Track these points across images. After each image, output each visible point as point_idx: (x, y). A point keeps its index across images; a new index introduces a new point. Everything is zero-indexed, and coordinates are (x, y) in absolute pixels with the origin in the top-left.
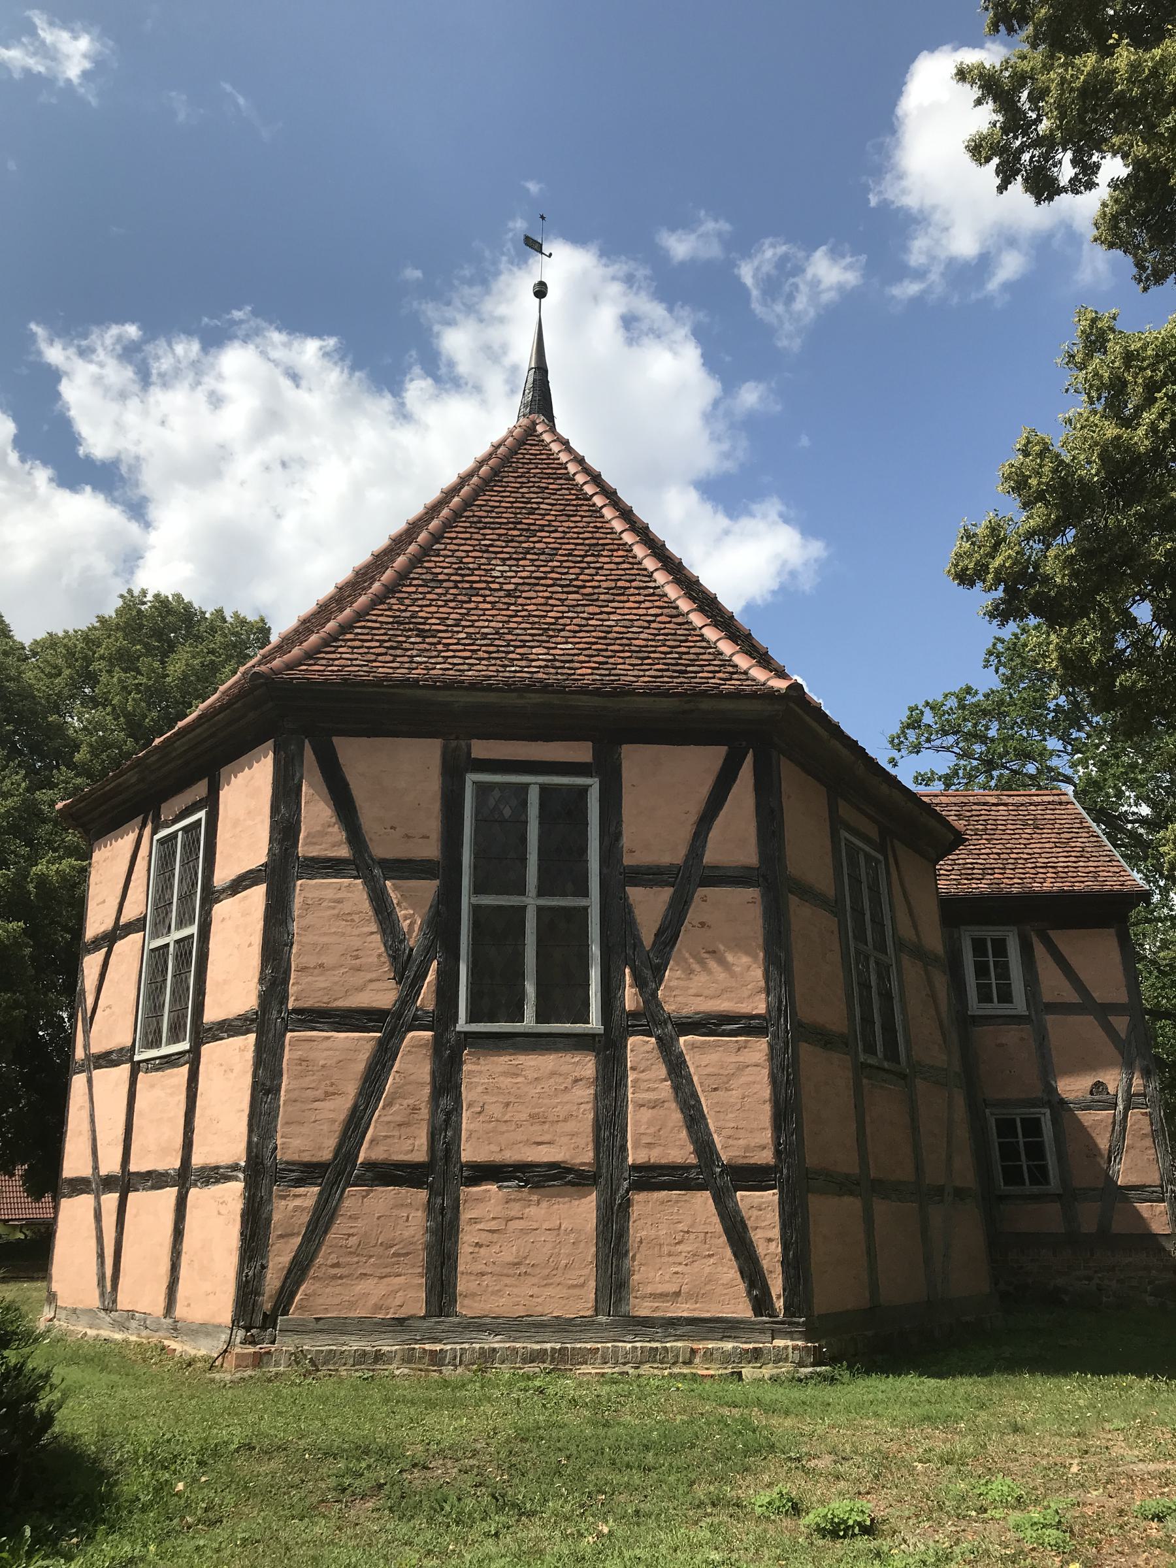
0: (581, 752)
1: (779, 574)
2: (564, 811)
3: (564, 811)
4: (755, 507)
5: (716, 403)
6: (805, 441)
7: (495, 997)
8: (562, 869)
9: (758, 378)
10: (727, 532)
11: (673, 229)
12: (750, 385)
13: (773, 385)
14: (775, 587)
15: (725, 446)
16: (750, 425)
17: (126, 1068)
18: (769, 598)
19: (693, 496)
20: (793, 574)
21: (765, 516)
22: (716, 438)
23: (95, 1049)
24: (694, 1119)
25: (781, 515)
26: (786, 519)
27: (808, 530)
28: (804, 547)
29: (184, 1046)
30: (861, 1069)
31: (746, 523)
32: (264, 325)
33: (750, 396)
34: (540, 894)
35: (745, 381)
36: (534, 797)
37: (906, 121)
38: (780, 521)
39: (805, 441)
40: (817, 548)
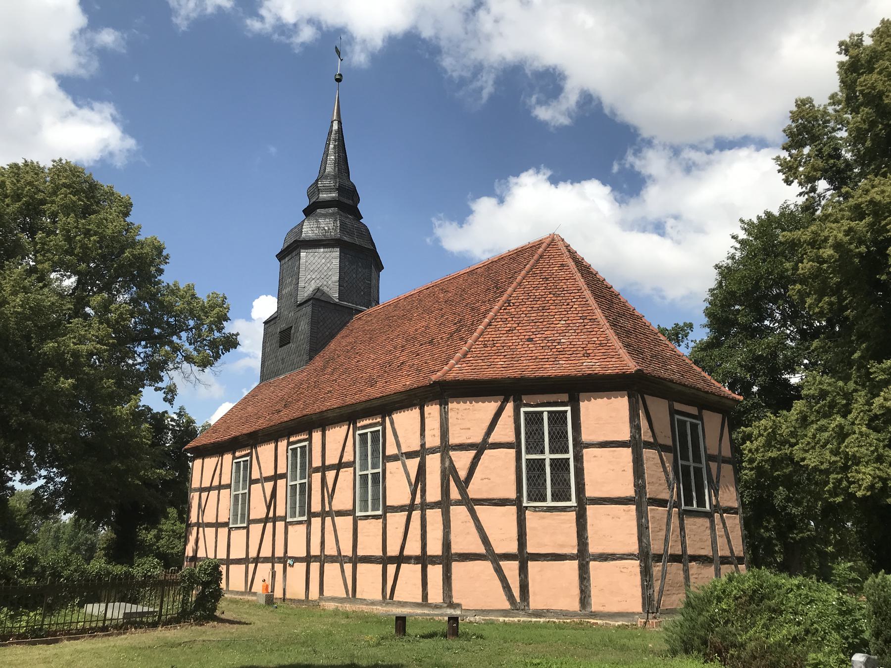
0: (565, 397)
1: (102, 151)
2: (557, 419)
3: (557, 419)
4: (97, 105)
5: (82, 31)
6: (137, 78)
7: (537, 495)
8: (559, 444)
9: (116, 27)
10: (72, 114)
11: (566, 126)
12: (111, 30)
13: (125, 36)
14: (98, 159)
15: (83, 60)
16: (103, 53)
17: (226, 529)
18: (92, 164)
19: (53, 84)
20: (111, 154)
21: (101, 112)
22: (76, 51)
23: (205, 521)
24: (683, 543)
25: (111, 115)
26: (114, 120)
27: (127, 130)
28: (122, 139)
29: (305, 518)
30: (682, 514)
31: (85, 112)
32: (276, 37)
33: (108, 37)
34: (542, 452)
35: (107, 26)
36: (545, 415)
37: (586, 89)
38: (110, 118)
39: (137, 78)
40: (131, 143)
